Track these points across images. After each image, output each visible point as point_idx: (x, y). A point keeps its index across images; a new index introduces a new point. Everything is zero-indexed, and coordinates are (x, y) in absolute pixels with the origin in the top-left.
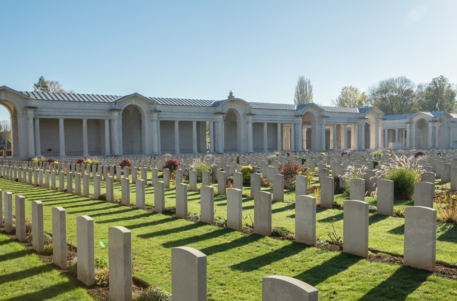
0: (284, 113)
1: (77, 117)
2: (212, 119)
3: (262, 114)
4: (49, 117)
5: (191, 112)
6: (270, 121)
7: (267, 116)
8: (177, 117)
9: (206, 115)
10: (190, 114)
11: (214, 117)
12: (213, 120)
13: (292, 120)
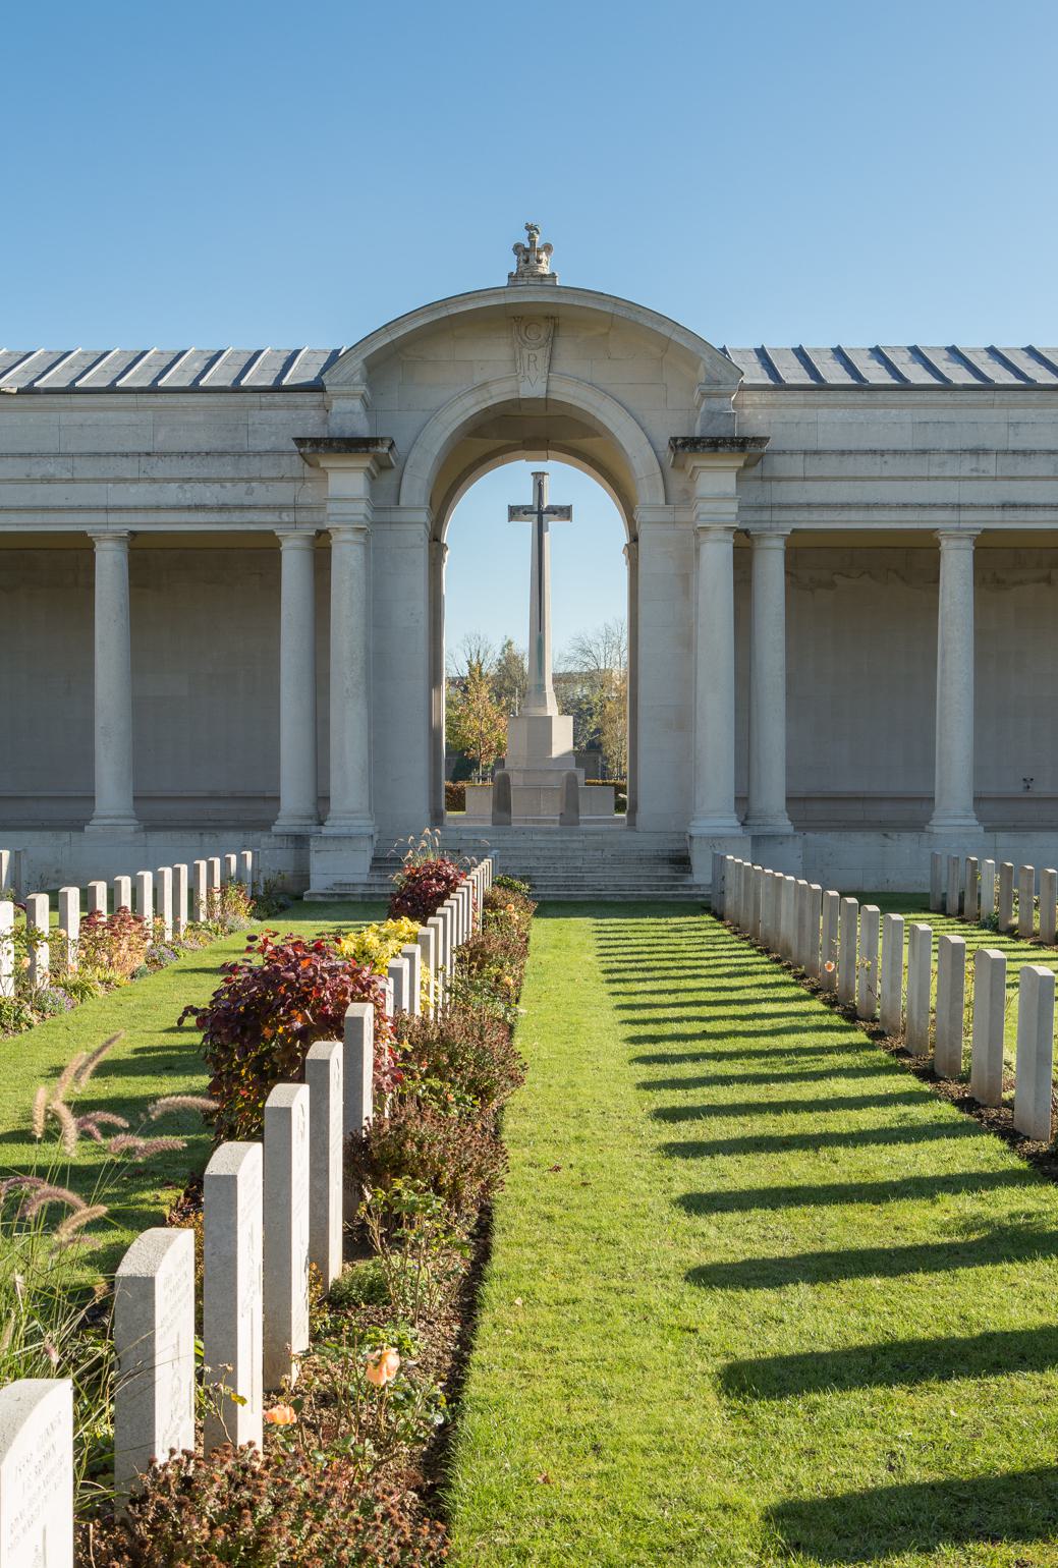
0: (119, 425)
1: (26, 518)
2: (296, 508)
3: (903, 439)
4: (252, 527)
5: (58, 455)
6: (1010, 515)
7: (967, 465)
8: (956, 502)
9: (226, 468)
10: (51, 468)
11: (309, 494)
12: (303, 515)
13: (283, 493)
